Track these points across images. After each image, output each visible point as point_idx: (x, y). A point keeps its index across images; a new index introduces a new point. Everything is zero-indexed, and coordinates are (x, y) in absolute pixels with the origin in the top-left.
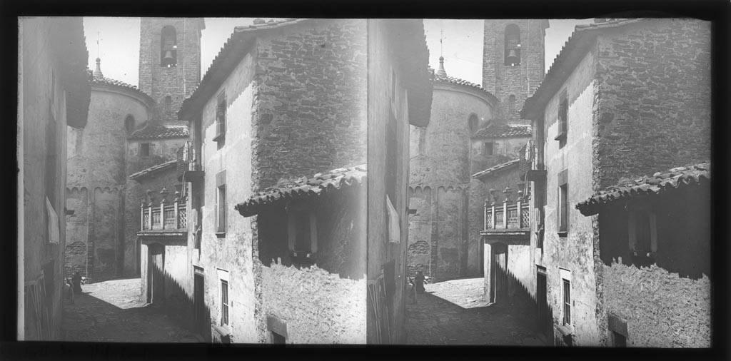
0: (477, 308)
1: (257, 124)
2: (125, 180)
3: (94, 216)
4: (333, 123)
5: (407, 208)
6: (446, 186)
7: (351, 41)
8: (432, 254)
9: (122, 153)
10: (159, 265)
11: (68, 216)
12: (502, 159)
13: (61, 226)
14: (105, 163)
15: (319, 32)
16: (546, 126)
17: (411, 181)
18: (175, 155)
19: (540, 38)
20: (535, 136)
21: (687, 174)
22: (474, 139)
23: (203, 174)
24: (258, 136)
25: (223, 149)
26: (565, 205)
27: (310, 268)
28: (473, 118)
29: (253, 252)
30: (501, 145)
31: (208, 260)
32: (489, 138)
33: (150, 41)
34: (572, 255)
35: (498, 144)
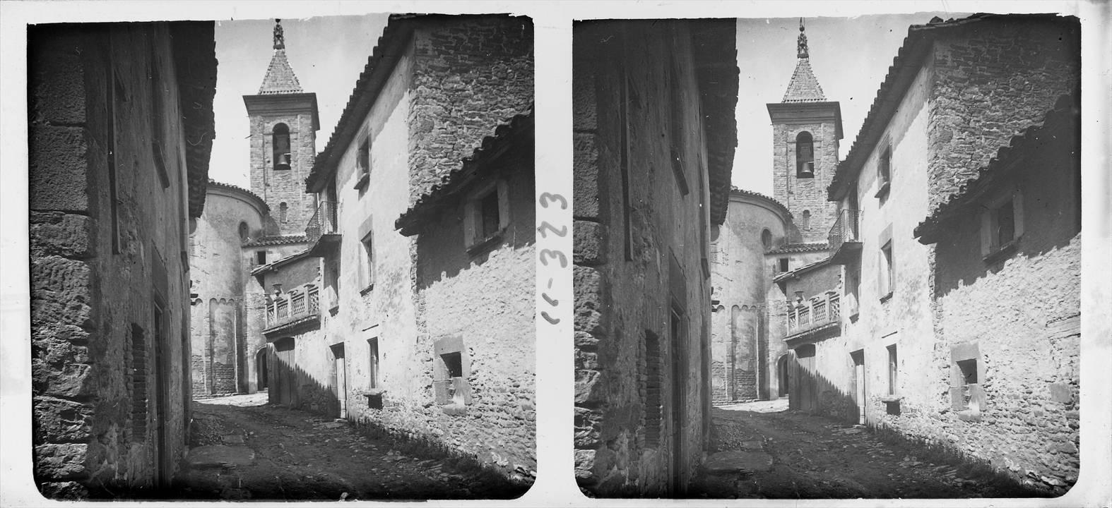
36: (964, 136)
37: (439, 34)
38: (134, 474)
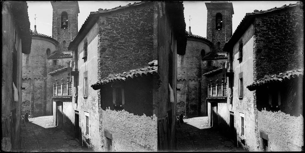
0: (205, 129)
1: (256, 53)
2: (201, 76)
3: (34, 90)
4: (287, 52)
5: (21, 87)
6: (192, 79)
7: (294, 18)
8: (186, 107)
9: (200, 65)
10: (215, 111)
11: (178, 91)
12: (60, 67)
13: (175, 95)
14: (193, 69)
15: (281, 15)
16: (78, 53)
17: (23, 76)
18: (222, 66)
19: (76, 17)
20: (74, 57)
21: (137, 72)
22: (49, 59)
23: (233, 73)
24: (256, 58)
25: (242, 63)
26: (87, 85)
27: (278, 112)
28: (48, 50)
29: (254, 105)
30: (60, 61)
31: (236, 109)
32: (55, 58)
33: (211, 19)
34: (89, 106)
35: (213, 62)
36: (110, 49)
37: (264, 19)
38: (232, 106)
